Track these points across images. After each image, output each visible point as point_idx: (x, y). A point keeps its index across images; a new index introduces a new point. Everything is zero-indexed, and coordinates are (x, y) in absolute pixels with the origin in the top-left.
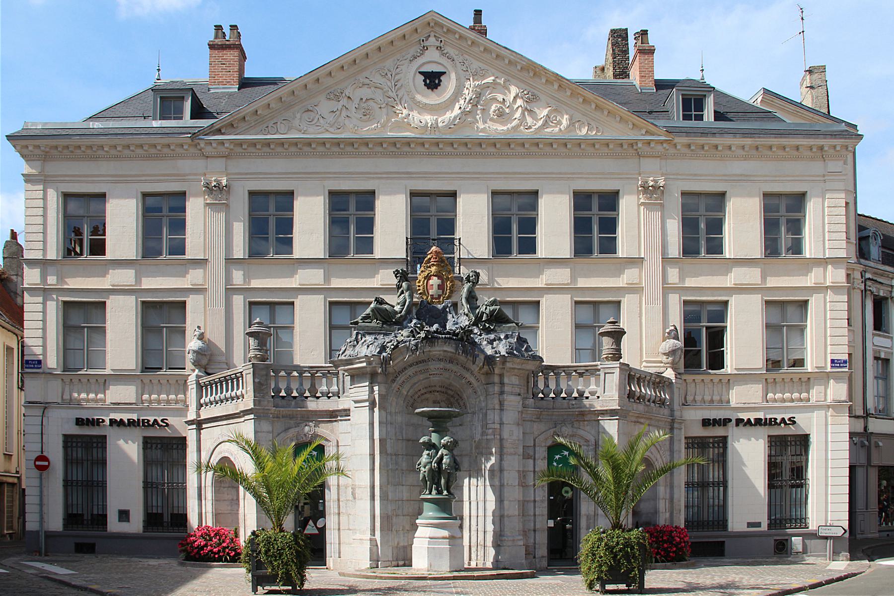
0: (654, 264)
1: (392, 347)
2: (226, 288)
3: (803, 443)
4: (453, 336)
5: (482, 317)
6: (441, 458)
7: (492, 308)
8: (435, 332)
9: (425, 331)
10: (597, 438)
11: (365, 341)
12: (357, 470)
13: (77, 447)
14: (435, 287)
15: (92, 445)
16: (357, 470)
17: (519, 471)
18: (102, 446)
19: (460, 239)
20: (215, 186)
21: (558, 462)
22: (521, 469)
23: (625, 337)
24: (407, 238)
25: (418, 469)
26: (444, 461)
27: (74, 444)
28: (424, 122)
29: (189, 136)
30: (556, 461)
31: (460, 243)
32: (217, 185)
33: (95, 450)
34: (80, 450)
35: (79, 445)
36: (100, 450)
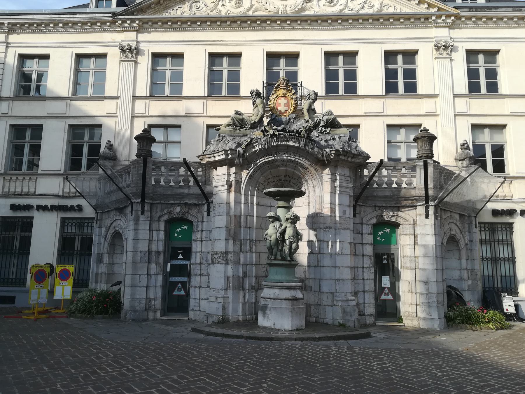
0: (446, 97)
1: (247, 143)
2: (131, 116)
3: (508, 229)
4: (296, 133)
5: (319, 122)
6: (285, 230)
7: (327, 117)
8: (281, 131)
9: (273, 129)
10: (415, 219)
11: (226, 140)
12: (216, 240)
13: (72, 226)
14: (283, 105)
15: (84, 225)
16: (216, 240)
17: (350, 243)
18: (92, 225)
19: (301, 82)
20: (128, 49)
21: (381, 237)
22: (352, 241)
23: (435, 142)
24: (263, 82)
25: (265, 238)
26: (287, 232)
27: (70, 224)
28: (277, 7)
29: (110, 15)
30: (379, 236)
31: (301, 85)
32: (129, 48)
33: (85, 228)
34: (74, 228)
35: (74, 224)
36: (89, 228)
